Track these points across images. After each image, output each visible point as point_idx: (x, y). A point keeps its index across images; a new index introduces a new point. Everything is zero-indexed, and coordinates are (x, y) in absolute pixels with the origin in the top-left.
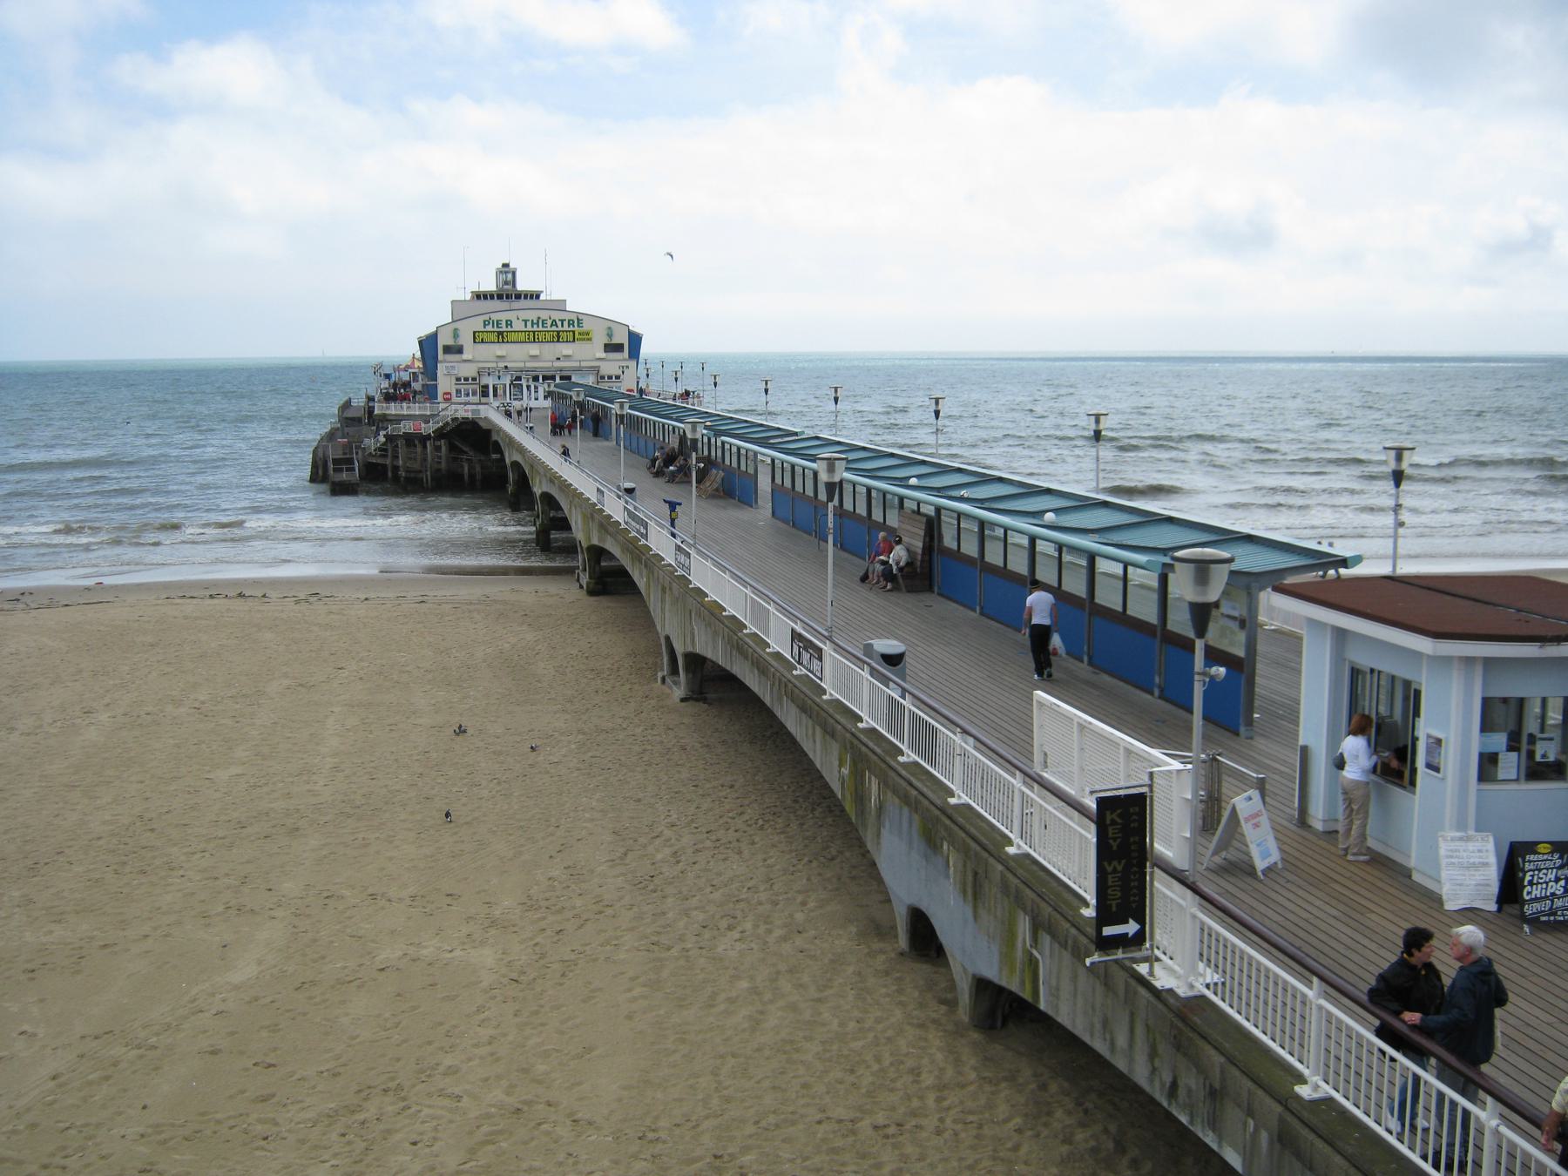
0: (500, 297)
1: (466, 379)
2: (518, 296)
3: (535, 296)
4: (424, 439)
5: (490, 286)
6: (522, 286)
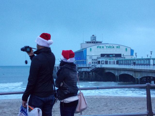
0: (93, 43)
1: (94, 60)
2: (97, 43)
4: (89, 72)
5: (90, 40)
6: (97, 40)
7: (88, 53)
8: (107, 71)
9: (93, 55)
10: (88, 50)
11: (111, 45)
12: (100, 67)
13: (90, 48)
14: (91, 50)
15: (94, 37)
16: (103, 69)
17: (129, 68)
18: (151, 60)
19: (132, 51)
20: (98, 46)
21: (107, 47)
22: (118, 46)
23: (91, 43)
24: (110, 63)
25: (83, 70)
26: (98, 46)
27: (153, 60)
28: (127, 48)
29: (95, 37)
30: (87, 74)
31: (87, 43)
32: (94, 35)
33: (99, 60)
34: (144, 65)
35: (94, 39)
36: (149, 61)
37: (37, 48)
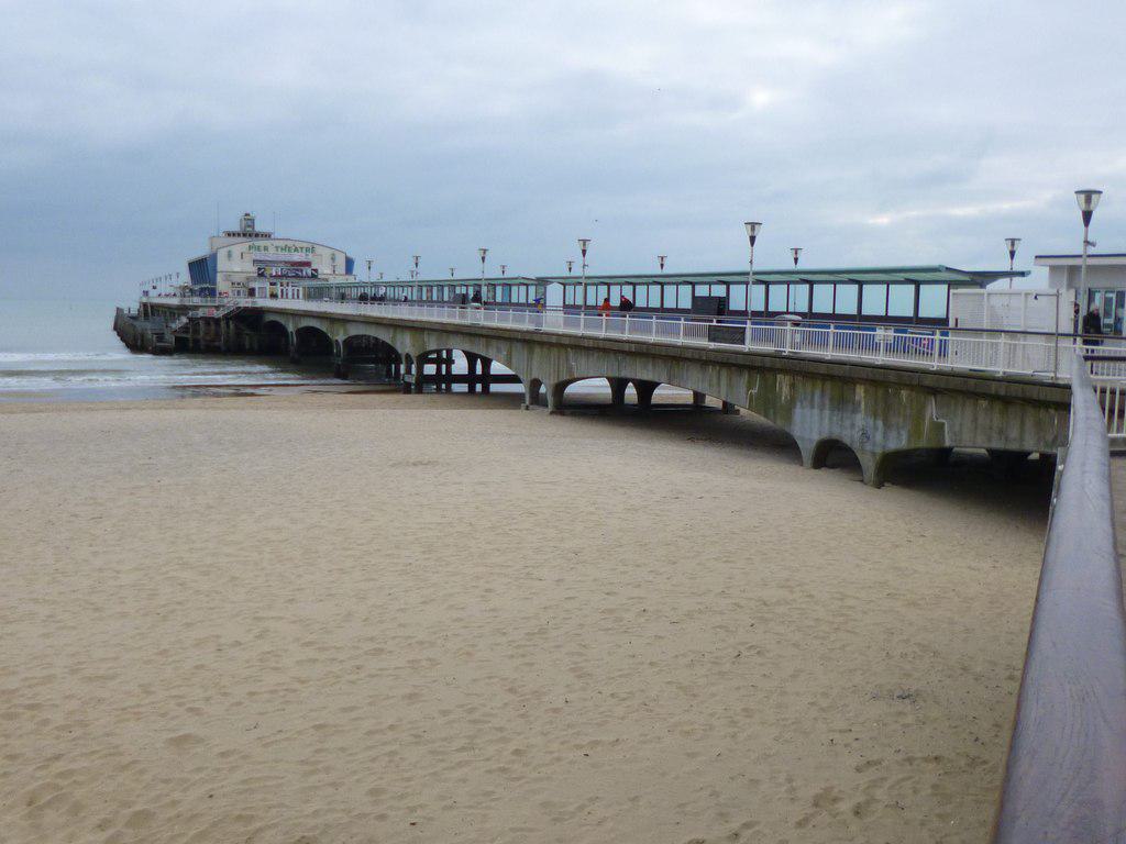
0: (244, 235)
1: (239, 284)
2: (257, 235)
3: (267, 236)
4: (217, 321)
5: (236, 228)
6: (259, 228)
7: (222, 264)
8: (270, 318)
9: (236, 270)
10: (221, 255)
11: (289, 244)
12: (250, 305)
13: (229, 248)
14: (229, 255)
15: (249, 220)
16: (258, 313)
17: (318, 310)
18: (549, 287)
19: (349, 264)
20: (251, 243)
21: (277, 247)
22: (310, 246)
23: (239, 235)
24: (875, 347)
25: (201, 313)
26: (251, 243)
27: (564, 285)
28: (336, 252)
29: (253, 220)
30: (213, 327)
31: (229, 235)
32: (246, 215)
33: (252, 285)
34: (420, 302)
35: (249, 226)
36: (541, 290)
37: (569, 394)
